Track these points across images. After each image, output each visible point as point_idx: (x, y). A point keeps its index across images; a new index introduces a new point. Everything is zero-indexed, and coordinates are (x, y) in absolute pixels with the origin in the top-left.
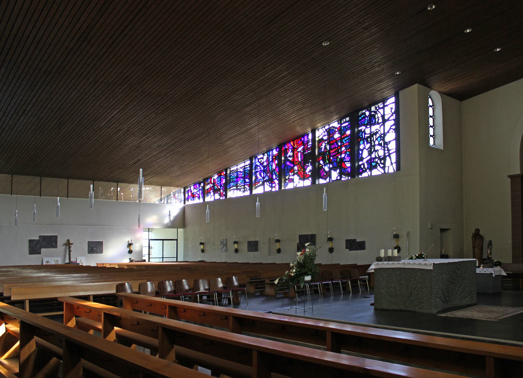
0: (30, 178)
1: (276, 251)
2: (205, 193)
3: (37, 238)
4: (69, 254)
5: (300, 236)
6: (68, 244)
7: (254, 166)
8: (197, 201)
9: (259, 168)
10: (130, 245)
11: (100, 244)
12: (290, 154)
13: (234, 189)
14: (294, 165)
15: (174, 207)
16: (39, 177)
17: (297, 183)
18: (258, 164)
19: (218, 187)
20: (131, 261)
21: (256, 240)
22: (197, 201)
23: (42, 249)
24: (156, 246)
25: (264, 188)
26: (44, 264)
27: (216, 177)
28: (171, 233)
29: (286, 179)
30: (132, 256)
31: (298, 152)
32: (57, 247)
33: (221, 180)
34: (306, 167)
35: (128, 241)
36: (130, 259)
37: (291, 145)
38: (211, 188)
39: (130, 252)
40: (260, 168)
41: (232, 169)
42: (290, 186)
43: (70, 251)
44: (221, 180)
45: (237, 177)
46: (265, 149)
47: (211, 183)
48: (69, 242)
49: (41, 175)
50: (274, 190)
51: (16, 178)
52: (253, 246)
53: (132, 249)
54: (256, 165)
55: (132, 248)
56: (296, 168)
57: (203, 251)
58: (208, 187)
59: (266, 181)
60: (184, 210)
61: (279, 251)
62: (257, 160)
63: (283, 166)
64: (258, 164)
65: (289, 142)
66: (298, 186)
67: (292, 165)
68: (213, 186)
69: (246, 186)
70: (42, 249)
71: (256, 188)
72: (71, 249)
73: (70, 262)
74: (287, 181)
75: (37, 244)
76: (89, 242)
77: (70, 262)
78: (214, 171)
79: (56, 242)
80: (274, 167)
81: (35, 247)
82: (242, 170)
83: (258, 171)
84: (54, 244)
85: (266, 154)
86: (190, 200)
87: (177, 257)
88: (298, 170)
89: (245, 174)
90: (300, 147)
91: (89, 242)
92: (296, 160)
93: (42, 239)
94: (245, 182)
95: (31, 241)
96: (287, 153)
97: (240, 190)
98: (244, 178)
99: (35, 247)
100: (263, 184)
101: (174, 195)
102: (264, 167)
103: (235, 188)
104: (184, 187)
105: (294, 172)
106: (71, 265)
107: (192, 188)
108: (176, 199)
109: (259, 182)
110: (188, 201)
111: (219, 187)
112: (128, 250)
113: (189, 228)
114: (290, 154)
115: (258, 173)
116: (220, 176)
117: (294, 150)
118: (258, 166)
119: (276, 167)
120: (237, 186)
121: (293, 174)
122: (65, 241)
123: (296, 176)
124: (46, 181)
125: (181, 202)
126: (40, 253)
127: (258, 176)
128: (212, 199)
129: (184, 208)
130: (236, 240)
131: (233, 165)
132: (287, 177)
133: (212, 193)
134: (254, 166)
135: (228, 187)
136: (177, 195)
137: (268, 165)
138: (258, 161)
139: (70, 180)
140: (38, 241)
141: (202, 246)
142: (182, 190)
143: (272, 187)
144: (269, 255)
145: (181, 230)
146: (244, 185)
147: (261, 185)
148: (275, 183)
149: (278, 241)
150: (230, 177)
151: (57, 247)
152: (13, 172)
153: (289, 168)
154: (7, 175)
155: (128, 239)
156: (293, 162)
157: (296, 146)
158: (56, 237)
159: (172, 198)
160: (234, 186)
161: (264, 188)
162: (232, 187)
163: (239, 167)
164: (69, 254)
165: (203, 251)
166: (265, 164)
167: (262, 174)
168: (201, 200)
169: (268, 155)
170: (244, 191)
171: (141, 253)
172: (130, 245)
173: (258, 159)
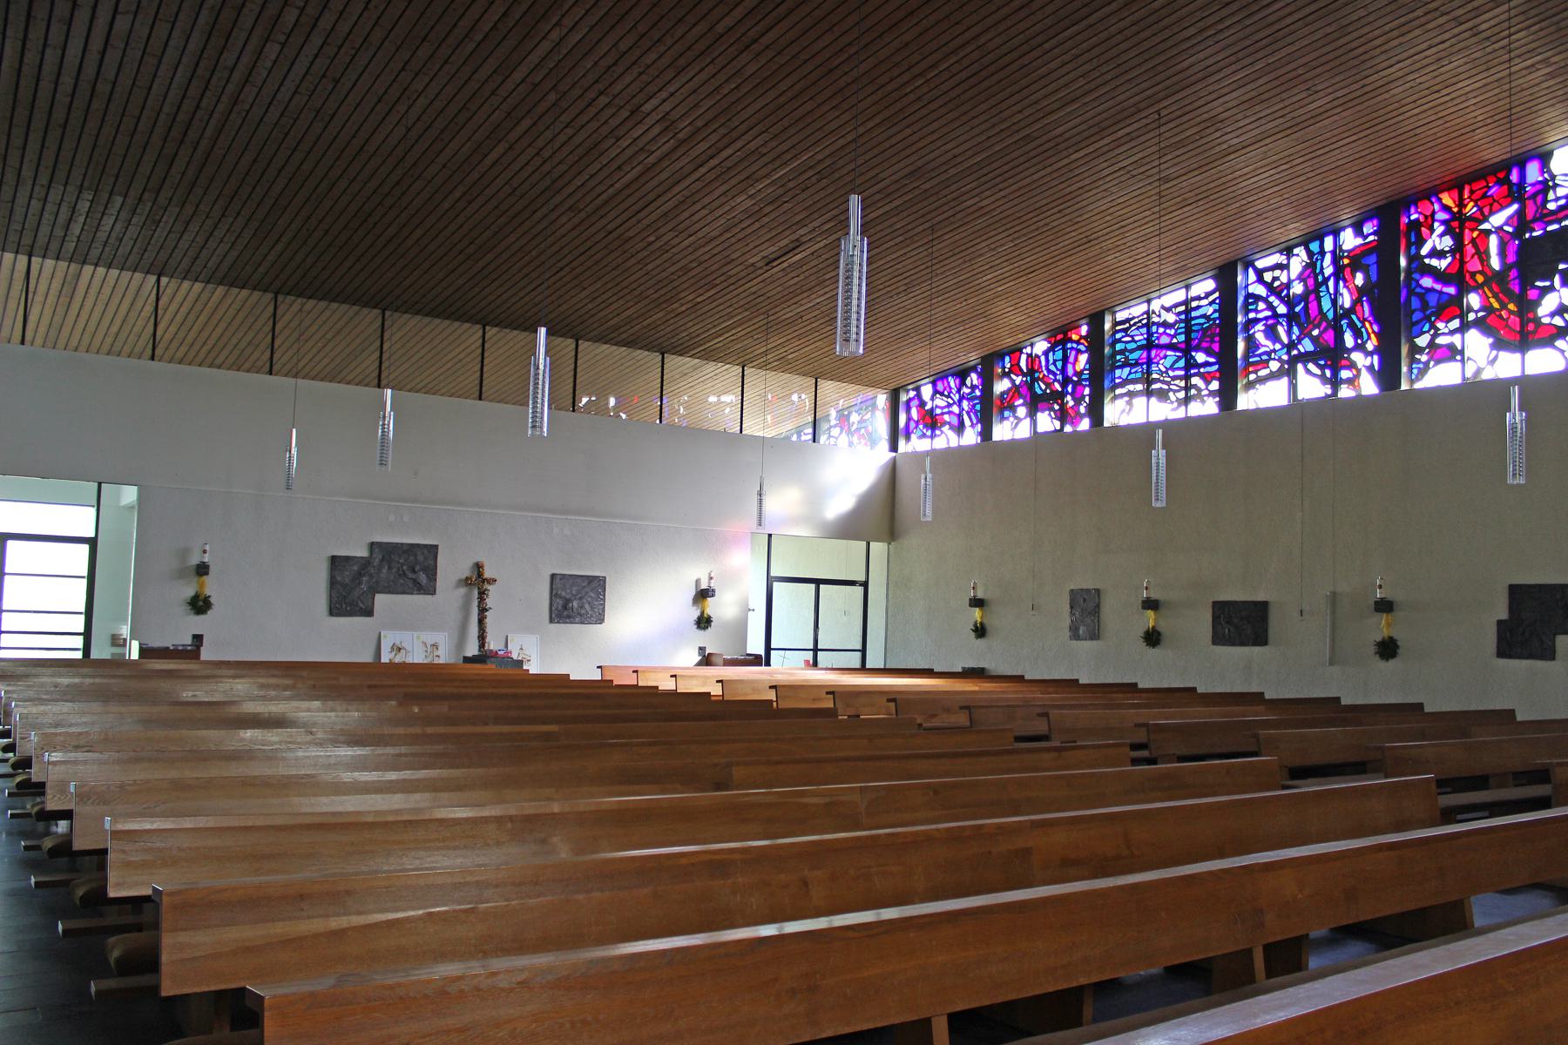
0: (341, 311)
1: (1372, 649)
2: (988, 410)
3: (363, 553)
4: (481, 621)
5: (1515, 591)
6: (478, 581)
7: (1241, 300)
8: (946, 439)
9: (1261, 306)
10: (703, 595)
11: (596, 586)
12: (1438, 240)
13: (1131, 394)
14: (1463, 289)
15: (852, 462)
16: (377, 311)
17: (1482, 363)
18: (1260, 290)
19: (1048, 385)
20: (707, 660)
21: (1260, 597)
22: (946, 439)
23: (378, 597)
24: (793, 604)
25: (1293, 387)
26: (385, 659)
27: (1041, 346)
28: (846, 558)
29: (1415, 350)
30: (711, 641)
31: (1488, 232)
32: (433, 592)
33: (1065, 359)
34: (1532, 294)
35: (698, 582)
36: (702, 649)
37: (1445, 208)
38: (1015, 391)
39: (704, 622)
40: (1271, 307)
41: (1120, 316)
42: (1443, 375)
43: (483, 611)
44: (1065, 359)
45: (1149, 346)
46: (1294, 231)
47: (1020, 372)
48: (480, 575)
49: (386, 300)
50: (1345, 392)
51: (291, 307)
52: (1242, 623)
53: (708, 612)
54: (1249, 296)
55: (712, 607)
56: (1474, 300)
57: (980, 631)
58: (1001, 386)
59: (1305, 358)
60: (892, 474)
61: (1388, 649)
62: (1252, 276)
63: (1404, 293)
64: (1260, 290)
65: (1431, 193)
66: (1487, 375)
67: (1451, 290)
68: (1030, 387)
69: (1195, 380)
70: (378, 597)
71: (1250, 386)
72: (489, 602)
73: (483, 657)
74: (1424, 358)
75: (360, 574)
76: (553, 576)
77: (483, 657)
78: (1034, 325)
79: (432, 572)
80: (1346, 300)
81: (351, 587)
82: (1171, 318)
83: (1257, 321)
84: (423, 578)
85: (1300, 251)
86: (913, 437)
87: (863, 651)
88: (1486, 307)
89: (1188, 331)
90: (1492, 213)
91: (553, 576)
92: (1474, 265)
93: (378, 556)
94: (1191, 365)
95: (335, 561)
96: (1421, 242)
97: (1163, 395)
98: (1186, 350)
99: (351, 587)
100: (1289, 371)
101: (843, 419)
102: (1290, 302)
103: (1139, 387)
104: (893, 386)
105: (1462, 316)
106: (490, 668)
107: (927, 391)
108: (849, 432)
109: (1265, 364)
110: (908, 439)
111: (1057, 386)
112: (696, 613)
113: (911, 542)
114: (1438, 240)
115: (1260, 327)
116: (1059, 338)
117: (1457, 225)
118: (1258, 298)
119: (1357, 302)
120: (1149, 382)
121: (1455, 324)
122: (465, 570)
123: (1473, 335)
124: (405, 326)
125: (873, 443)
126: (368, 612)
127: (1260, 337)
128: (1024, 431)
129: (894, 463)
130: (1154, 596)
131: (1125, 302)
132: (1422, 341)
133: (1022, 411)
134: (1241, 300)
135: (1107, 383)
136: (854, 418)
137: (1313, 293)
138: (1260, 280)
139: (491, 331)
140: (365, 563)
141: (977, 614)
142: (882, 399)
143: (1335, 383)
144: (1331, 663)
145: (878, 548)
146: (1187, 377)
147: (1273, 376)
148: (1351, 365)
149: (1385, 606)
150: (1113, 345)
151: (433, 592)
152: (280, 285)
153: (1432, 300)
154: (257, 294)
155: (695, 572)
156: (1459, 278)
157: (1470, 209)
158: (433, 549)
159: (836, 432)
160: (1134, 381)
161: (1293, 387)
162: (1121, 385)
163: (1156, 305)
164: (481, 621)
165: (980, 631)
166: (1298, 288)
167: (1281, 331)
168: (971, 437)
169: (1310, 254)
170: (1187, 401)
171: (740, 630)
172: (703, 595)
173: (1259, 274)
